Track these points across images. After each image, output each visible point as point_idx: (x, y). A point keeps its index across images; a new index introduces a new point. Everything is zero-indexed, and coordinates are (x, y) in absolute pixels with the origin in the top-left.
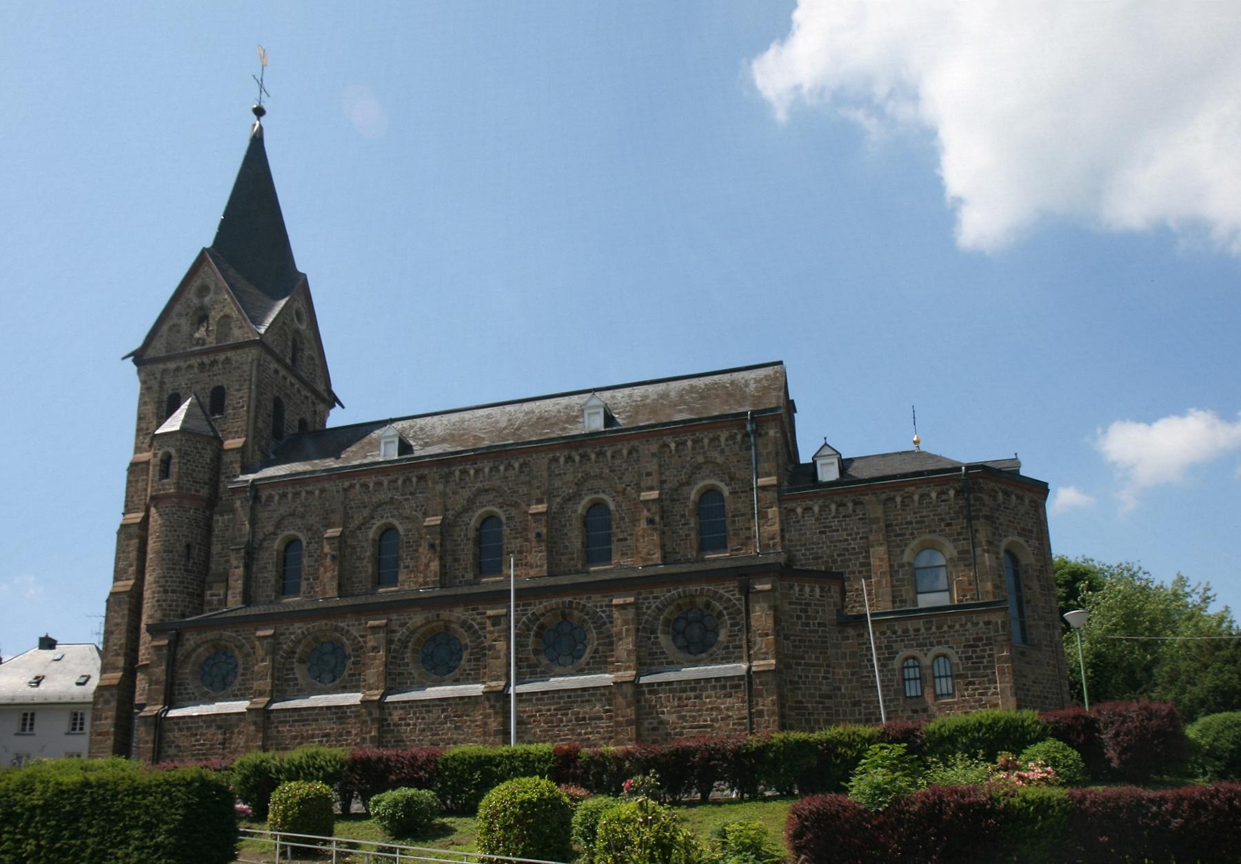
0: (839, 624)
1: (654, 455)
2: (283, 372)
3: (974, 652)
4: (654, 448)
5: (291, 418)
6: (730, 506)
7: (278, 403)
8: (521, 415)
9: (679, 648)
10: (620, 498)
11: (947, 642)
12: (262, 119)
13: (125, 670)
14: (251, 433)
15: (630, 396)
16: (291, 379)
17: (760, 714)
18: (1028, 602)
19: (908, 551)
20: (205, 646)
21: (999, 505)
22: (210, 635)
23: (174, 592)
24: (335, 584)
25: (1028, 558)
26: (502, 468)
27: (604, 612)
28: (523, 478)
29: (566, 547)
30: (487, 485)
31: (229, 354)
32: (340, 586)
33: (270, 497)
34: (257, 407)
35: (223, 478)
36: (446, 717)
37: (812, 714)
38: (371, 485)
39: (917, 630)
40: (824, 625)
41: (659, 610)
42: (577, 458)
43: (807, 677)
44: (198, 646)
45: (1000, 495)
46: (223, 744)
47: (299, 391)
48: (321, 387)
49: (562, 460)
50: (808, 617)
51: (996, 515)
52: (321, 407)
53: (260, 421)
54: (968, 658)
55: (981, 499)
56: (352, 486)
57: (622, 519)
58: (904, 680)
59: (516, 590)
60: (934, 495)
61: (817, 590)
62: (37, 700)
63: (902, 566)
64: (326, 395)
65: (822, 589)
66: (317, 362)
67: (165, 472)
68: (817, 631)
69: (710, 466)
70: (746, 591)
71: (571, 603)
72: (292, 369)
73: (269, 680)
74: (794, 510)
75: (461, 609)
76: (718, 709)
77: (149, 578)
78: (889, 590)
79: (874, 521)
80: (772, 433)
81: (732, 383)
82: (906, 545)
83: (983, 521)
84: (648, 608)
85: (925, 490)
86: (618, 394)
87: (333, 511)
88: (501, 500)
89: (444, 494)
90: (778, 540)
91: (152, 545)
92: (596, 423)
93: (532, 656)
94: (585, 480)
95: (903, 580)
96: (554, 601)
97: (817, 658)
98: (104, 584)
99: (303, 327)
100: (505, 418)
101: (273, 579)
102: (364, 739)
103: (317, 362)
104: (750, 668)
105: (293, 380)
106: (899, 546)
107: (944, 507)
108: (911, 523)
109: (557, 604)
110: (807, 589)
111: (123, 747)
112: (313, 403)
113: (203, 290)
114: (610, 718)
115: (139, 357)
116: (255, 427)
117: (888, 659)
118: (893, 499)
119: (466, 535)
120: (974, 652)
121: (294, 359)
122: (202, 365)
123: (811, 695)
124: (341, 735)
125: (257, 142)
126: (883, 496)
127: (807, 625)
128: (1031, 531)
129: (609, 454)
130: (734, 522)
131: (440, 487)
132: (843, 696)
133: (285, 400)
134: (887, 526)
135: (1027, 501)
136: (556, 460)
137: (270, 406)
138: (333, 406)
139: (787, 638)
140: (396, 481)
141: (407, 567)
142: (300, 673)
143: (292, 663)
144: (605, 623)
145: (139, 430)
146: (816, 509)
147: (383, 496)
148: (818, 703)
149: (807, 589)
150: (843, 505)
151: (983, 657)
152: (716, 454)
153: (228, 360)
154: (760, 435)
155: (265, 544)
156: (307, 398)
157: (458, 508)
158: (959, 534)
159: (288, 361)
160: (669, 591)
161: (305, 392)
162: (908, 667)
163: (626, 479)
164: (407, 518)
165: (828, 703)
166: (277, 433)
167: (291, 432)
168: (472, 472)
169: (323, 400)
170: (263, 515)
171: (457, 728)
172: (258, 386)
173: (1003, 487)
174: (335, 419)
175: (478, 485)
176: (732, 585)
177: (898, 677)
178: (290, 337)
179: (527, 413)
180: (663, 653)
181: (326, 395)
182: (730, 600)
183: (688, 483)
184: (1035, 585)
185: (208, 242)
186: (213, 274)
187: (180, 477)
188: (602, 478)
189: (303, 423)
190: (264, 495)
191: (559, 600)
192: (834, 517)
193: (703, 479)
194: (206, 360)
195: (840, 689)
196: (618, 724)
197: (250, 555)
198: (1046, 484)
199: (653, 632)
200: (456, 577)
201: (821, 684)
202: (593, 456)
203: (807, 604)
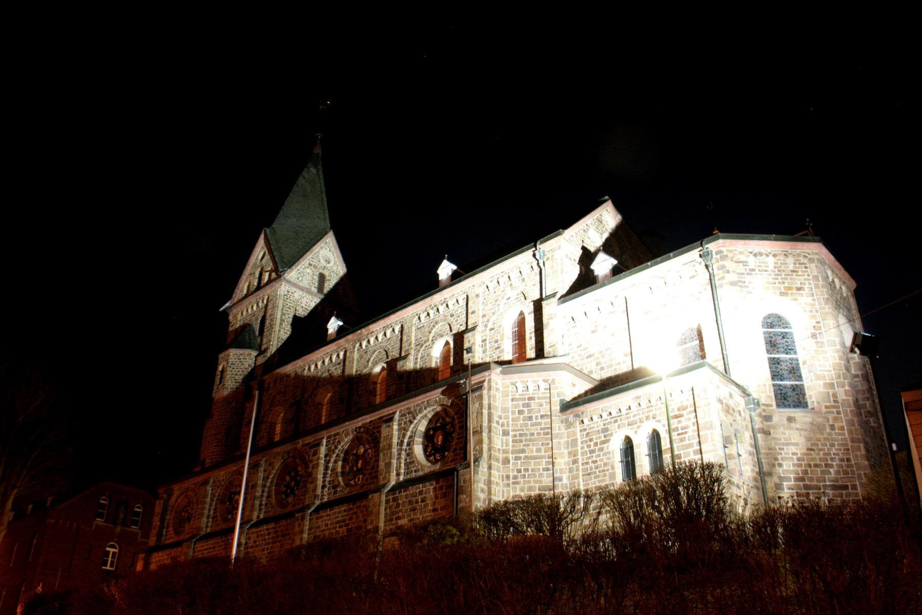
117: (604, 442)
127: (530, 418)
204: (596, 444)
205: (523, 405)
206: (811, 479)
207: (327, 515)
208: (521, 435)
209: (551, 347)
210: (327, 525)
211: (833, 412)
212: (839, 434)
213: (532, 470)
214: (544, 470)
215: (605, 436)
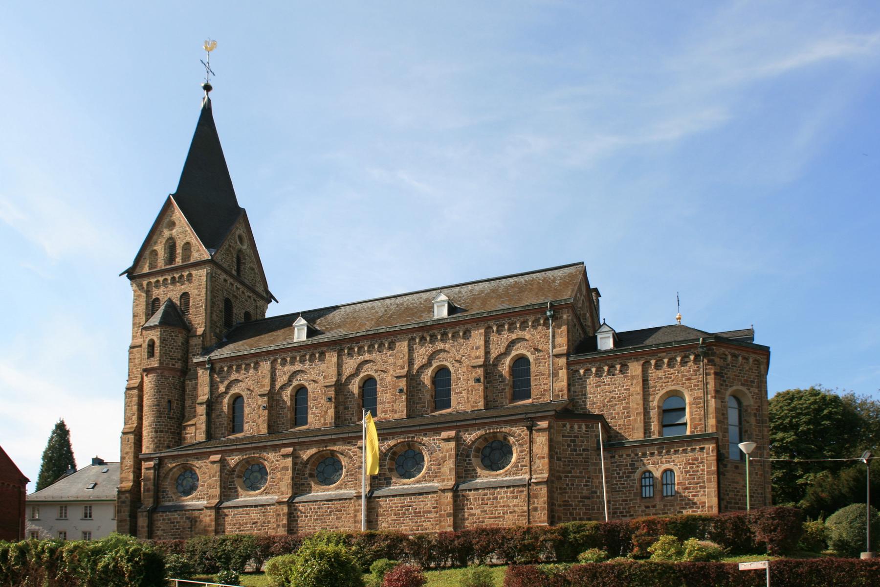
2: (230, 280)
6: (533, 368)
7: (228, 304)
8: (394, 307)
13: (134, 481)
14: (208, 324)
15: (471, 291)
16: (236, 284)
17: (535, 509)
18: (746, 431)
21: (728, 365)
24: (266, 425)
25: (749, 401)
29: (420, 399)
32: (269, 427)
33: (222, 368)
35: (190, 355)
36: (331, 512)
37: (575, 509)
45: (729, 357)
46: (191, 528)
47: (243, 292)
48: (260, 289)
50: (575, 446)
51: (726, 371)
52: (260, 303)
53: (214, 315)
54: (687, 472)
58: (642, 486)
61: (584, 427)
62: (92, 498)
64: (265, 295)
65: (587, 426)
66: (257, 271)
67: (151, 354)
68: (582, 455)
72: (238, 278)
73: (218, 489)
74: (578, 371)
76: (509, 506)
77: (146, 423)
78: (642, 424)
80: (565, 317)
81: (544, 280)
86: (464, 289)
90: (565, 392)
91: (147, 401)
92: (441, 312)
93: (387, 472)
97: (581, 472)
98: (119, 425)
100: (383, 309)
102: (278, 526)
103: (257, 271)
104: (530, 479)
105: (238, 286)
110: (576, 427)
111: (134, 532)
112: (255, 300)
114: (437, 512)
115: (131, 274)
116: (211, 320)
117: (632, 473)
121: (238, 271)
123: (575, 497)
124: (264, 523)
125: (207, 113)
127: (575, 450)
128: (752, 382)
133: (233, 300)
135: (751, 360)
139: (559, 459)
141: (314, 413)
142: (238, 483)
145: (134, 324)
149: (576, 427)
151: (697, 471)
154: (557, 318)
155: (219, 399)
156: (249, 297)
159: (234, 272)
162: (645, 478)
163: (462, 351)
165: (587, 502)
166: (228, 323)
167: (238, 321)
169: (262, 298)
171: (337, 518)
173: (733, 351)
174: (272, 311)
177: (637, 484)
178: (235, 256)
179: (398, 305)
181: (265, 295)
184: (752, 420)
187: (161, 356)
189: (247, 315)
190: (217, 366)
196: (441, 516)
198: (768, 348)
199: (468, 456)
200: (346, 420)
201: (582, 489)
203: (575, 437)
204: (624, 473)
210: (391, 507)
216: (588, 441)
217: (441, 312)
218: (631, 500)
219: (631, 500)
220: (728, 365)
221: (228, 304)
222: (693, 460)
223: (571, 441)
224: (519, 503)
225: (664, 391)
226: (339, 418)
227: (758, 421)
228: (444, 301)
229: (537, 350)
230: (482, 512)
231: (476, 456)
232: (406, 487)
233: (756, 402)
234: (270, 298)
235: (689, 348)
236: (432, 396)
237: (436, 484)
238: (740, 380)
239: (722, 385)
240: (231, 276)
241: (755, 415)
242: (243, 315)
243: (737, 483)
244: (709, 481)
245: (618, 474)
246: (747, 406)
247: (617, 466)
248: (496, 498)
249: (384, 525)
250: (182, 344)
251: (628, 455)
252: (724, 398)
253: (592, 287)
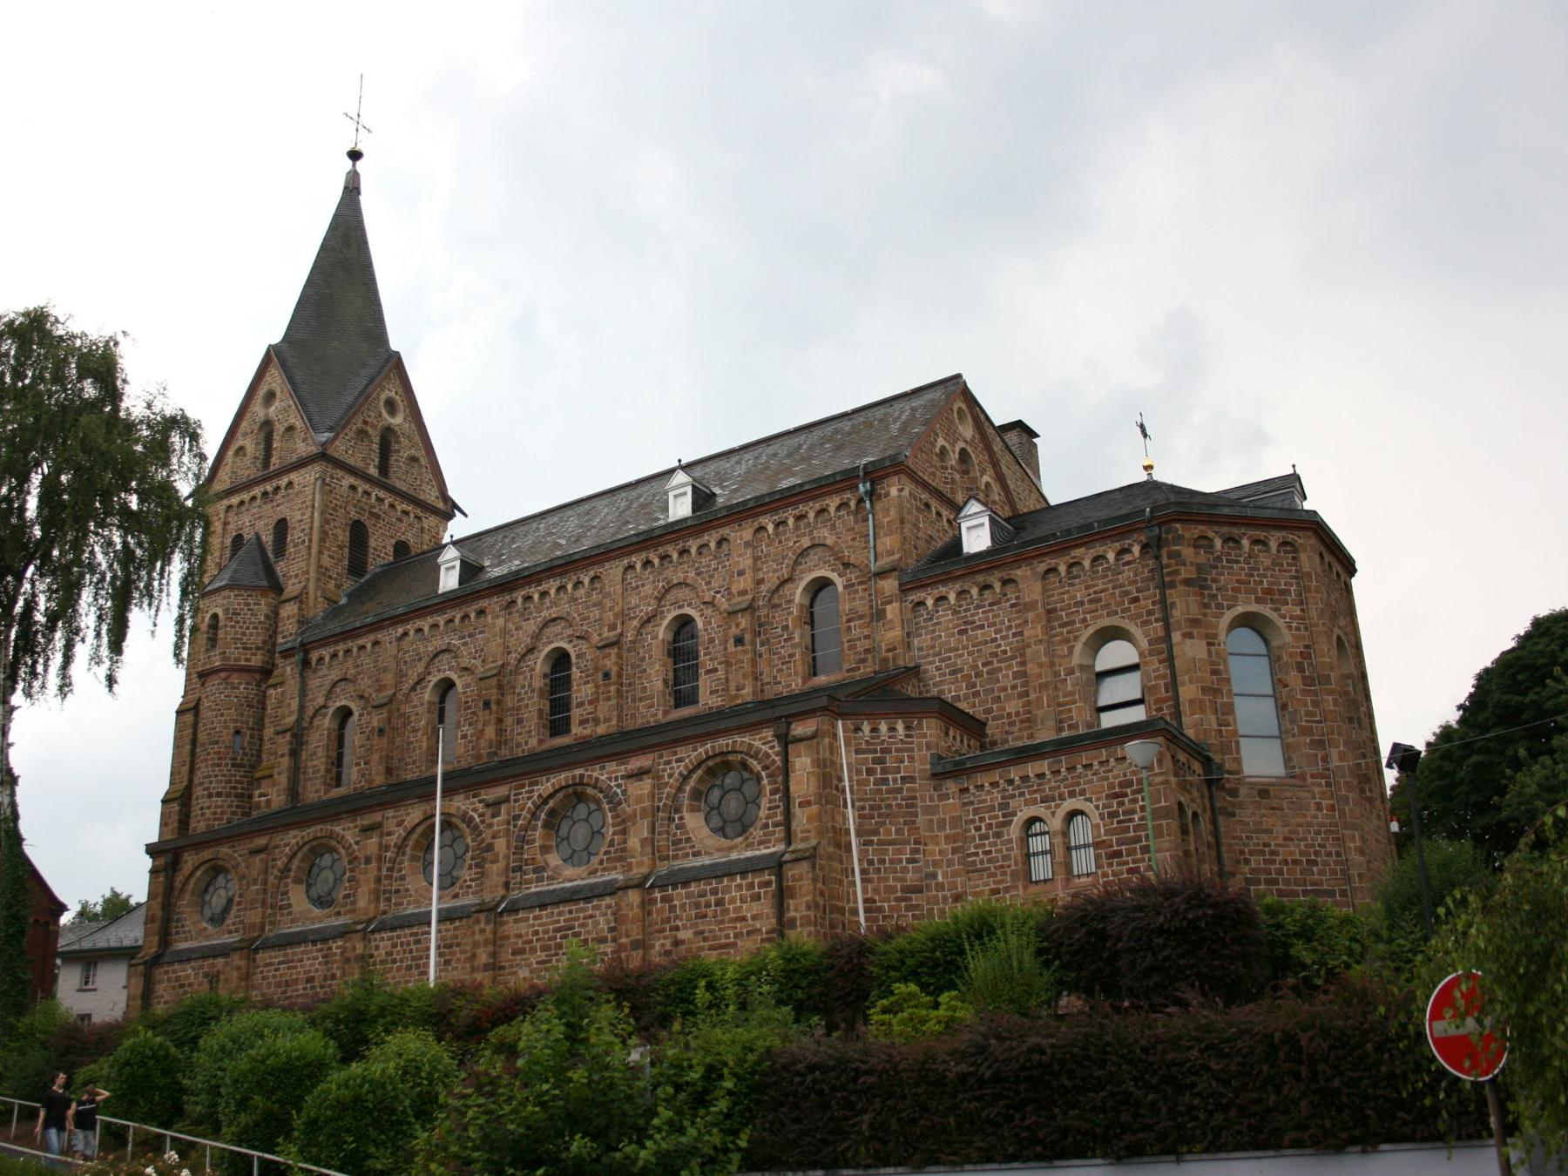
0: (935, 776)
1: (747, 544)
2: (363, 486)
3: (1121, 804)
4: (747, 534)
5: (380, 549)
7: (358, 534)
9: (714, 831)
10: (709, 611)
11: (1082, 793)
12: (358, 163)
16: (376, 492)
19: (1079, 646)
20: (203, 868)
22: (207, 854)
23: (219, 795)
26: (570, 587)
27: (619, 786)
28: (595, 597)
30: (554, 613)
31: (293, 476)
33: (321, 659)
34: (322, 540)
38: (426, 629)
39: (1041, 776)
40: (912, 779)
41: (685, 778)
42: (656, 561)
43: (882, 861)
44: (196, 869)
45: (1218, 543)
47: (392, 506)
48: (431, 496)
49: (638, 566)
50: (884, 771)
52: (430, 521)
53: (325, 556)
54: (1112, 815)
55: (1178, 554)
56: (405, 634)
57: (711, 641)
59: (444, 774)
60: (1111, 556)
61: (900, 726)
63: (1071, 672)
65: (908, 728)
68: (900, 790)
69: (819, 549)
70: (785, 741)
71: (582, 776)
72: (382, 479)
74: (922, 603)
75: (462, 797)
76: (743, 919)
79: (1031, 606)
80: (894, 492)
82: (1076, 638)
83: (1181, 588)
84: (670, 776)
85: (1098, 550)
87: (385, 670)
88: (569, 631)
89: (505, 632)
92: (681, 508)
94: (667, 591)
95: (1071, 693)
96: (563, 776)
97: (899, 831)
99: (397, 420)
101: (322, 768)
103: (423, 461)
105: (381, 494)
106: (1067, 641)
107: (1127, 573)
108: (1082, 603)
109: (566, 779)
110: (883, 727)
112: (417, 517)
113: (270, 396)
117: (1003, 825)
118: (1053, 570)
119: (530, 685)
120: (1121, 804)
121: (384, 467)
122: (265, 494)
125: (352, 190)
126: (1042, 567)
127: (885, 781)
128: (1282, 592)
129: (693, 551)
130: (849, 628)
131: (500, 622)
132: (940, 887)
134: (1049, 612)
135: (1273, 545)
136: (631, 567)
137: (344, 537)
138: (451, 516)
140: (451, 621)
143: (287, 885)
144: (620, 803)
146: (952, 597)
147: (438, 643)
148: (898, 900)
149: (883, 727)
150: (987, 587)
151: (1133, 812)
152: (825, 532)
153: (290, 484)
155: (316, 722)
157: (522, 648)
158: (1150, 613)
160: (695, 749)
161: (401, 506)
164: (466, 669)
165: (915, 899)
166: (357, 567)
168: (536, 597)
169: (434, 511)
170: (313, 683)
172: (322, 513)
175: (545, 613)
176: (768, 734)
177: (1016, 852)
178: (377, 440)
180: (688, 840)
181: (441, 505)
182: (768, 755)
183: (790, 580)
185: (277, 337)
186: (275, 380)
188: (687, 585)
189: (401, 548)
191: (568, 774)
192: (978, 607)
193: (811, 571)
194: (269, 487)
195: (934, 876)
197: (298, 737)
201: (904, 870)
202: (675, 556)
203: (883, 751)
204: (989, 826)
205: (875, 761)
206: (1287, 882)
207: (535, 918)
208: (872, 808)
209: (889, 650)
210: (536, 933)
211: (1319, 784)
212: (1327, 817)
213: (892, 861)
214: (909, 861)
215: (1004, 816)
216: (911, 759)
217: (681, 508)
218: (1006, 890)
219: (1006, 890)
220: (1219, 559)
221: (358, 534)
222: (1121, 785)
223: (875, 761)
224: (760, 912)
225: (1091, 630)
226: (1284, 707)
227: (1308, 681)
228: (683, 485)
229: (846, 565)
230: (696, 933)
231: (693, 809)
232: (569, 885)
233: (1297, 638)
234: (449, 509)
235: (1127, 532)
236: (665, 681)
237: (617, 876)
238: (1254, 591)
239: (1206, 606)
240: (367, 478)
241: (1300, 669)
242: (390, 549)
243: (1269, 831)
244: (1158, 833)
245: (978, 829)
246: (1280, 647)
247: (976, 811)
248: (719, 903)
249: (524, 973)
250: (267, 617)
251: (994, 784)
252: (1216, 636)
253: (999, 417)
